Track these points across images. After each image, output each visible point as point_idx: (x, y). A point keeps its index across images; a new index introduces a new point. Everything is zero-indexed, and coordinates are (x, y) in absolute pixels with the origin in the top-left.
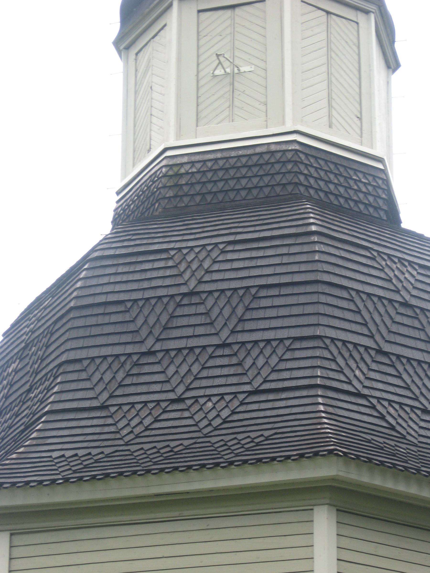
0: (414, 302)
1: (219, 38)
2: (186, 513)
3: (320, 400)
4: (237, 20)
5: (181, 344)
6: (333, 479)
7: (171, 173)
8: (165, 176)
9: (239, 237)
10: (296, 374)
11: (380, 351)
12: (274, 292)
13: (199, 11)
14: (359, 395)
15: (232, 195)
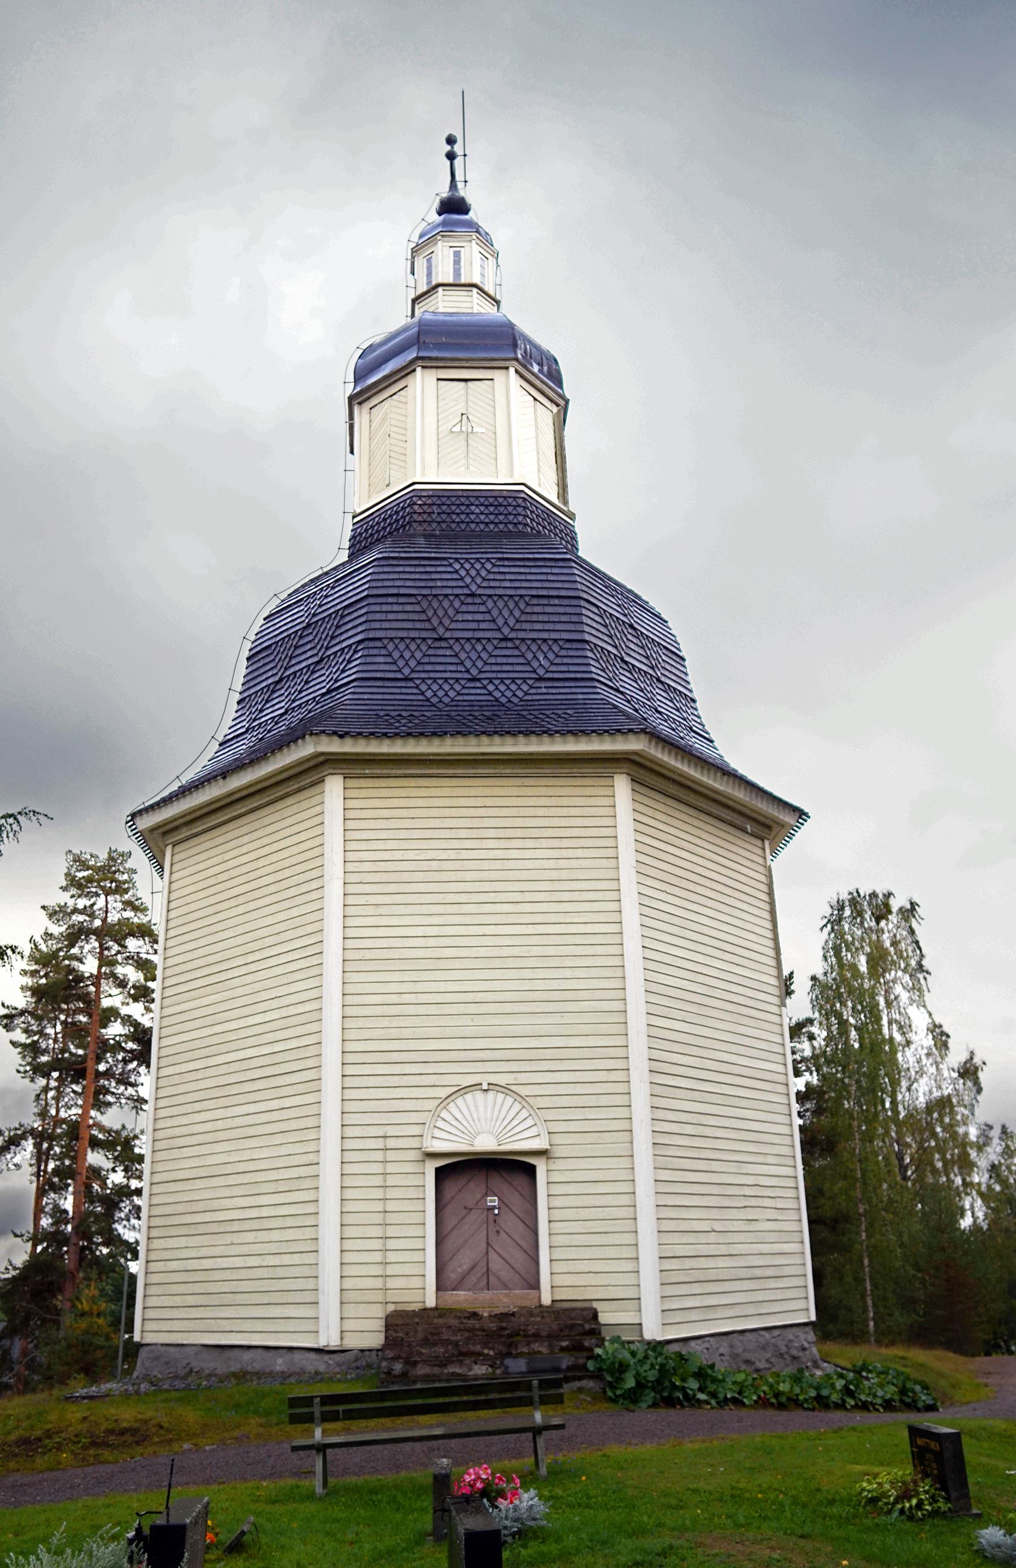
0: (636, 626)
1: (454, 403)
2: (480, 771)
4: (470, 391)
6: (635, 753)
9: (505, 556)
10: (572, 668)
11: (622, 659)
12: (545, 601)
13: (438, 379)
15: (473, 526)
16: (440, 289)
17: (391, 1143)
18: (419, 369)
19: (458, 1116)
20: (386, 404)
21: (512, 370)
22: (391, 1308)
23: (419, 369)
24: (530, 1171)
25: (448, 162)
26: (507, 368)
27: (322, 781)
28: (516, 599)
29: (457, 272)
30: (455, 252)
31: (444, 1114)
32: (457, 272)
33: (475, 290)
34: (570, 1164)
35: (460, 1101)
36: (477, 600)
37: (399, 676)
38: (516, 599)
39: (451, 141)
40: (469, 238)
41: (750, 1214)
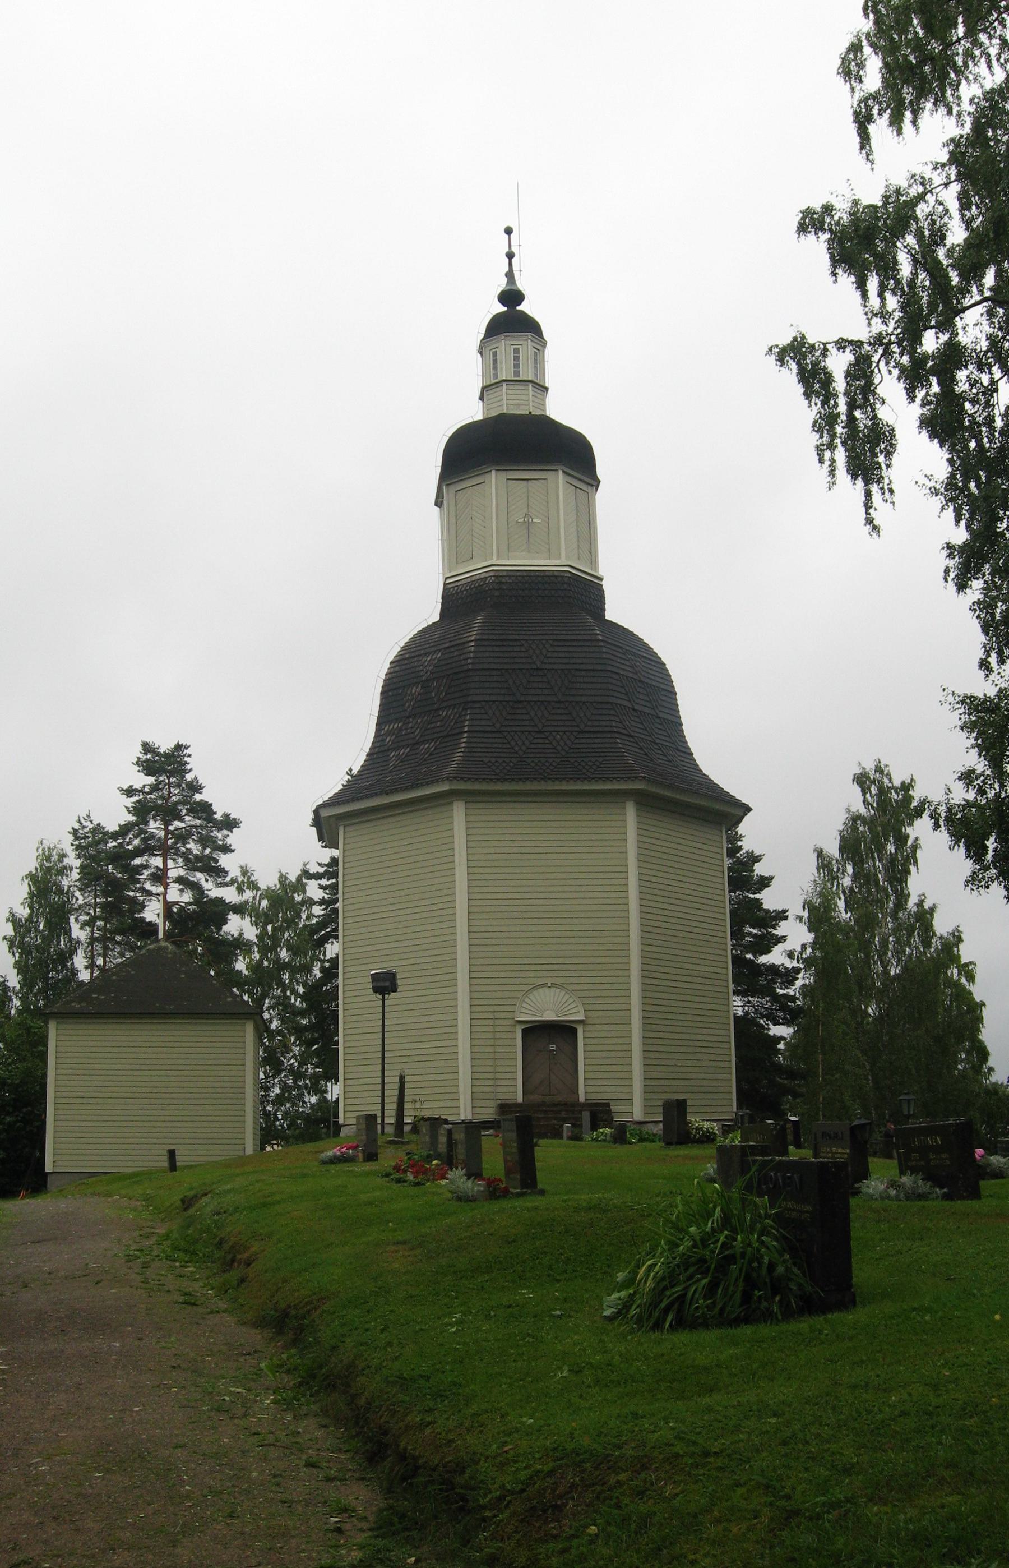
3: (618, 741)
5: (535, 699)
6: (643, 790)
7: (497, 581)
8: (493, 582)
14: (632, 737)
16: (504, 384)
17: (497, 1015)
18: (493, 472)
19: (535, 1001)
20: (469, 491)
21: (561, 472)
22: (499, 1102)
23: (493, 472)
24: (574, 1032)
25: (507, 260)
26: (557, 470)
27: (451, 803)
28: (566, 672)
29: (517, 373)
30: (519, 376)
31: (527, 1000)
32: (517, 373)
33: (530, 385)
34: (598, 1027)
35: (535, 993)
36: (540, 673)
37: (494, 729)
38: (566, 672)
39: (509, 231)
40: (525, 337)
41: (699, 1057)
